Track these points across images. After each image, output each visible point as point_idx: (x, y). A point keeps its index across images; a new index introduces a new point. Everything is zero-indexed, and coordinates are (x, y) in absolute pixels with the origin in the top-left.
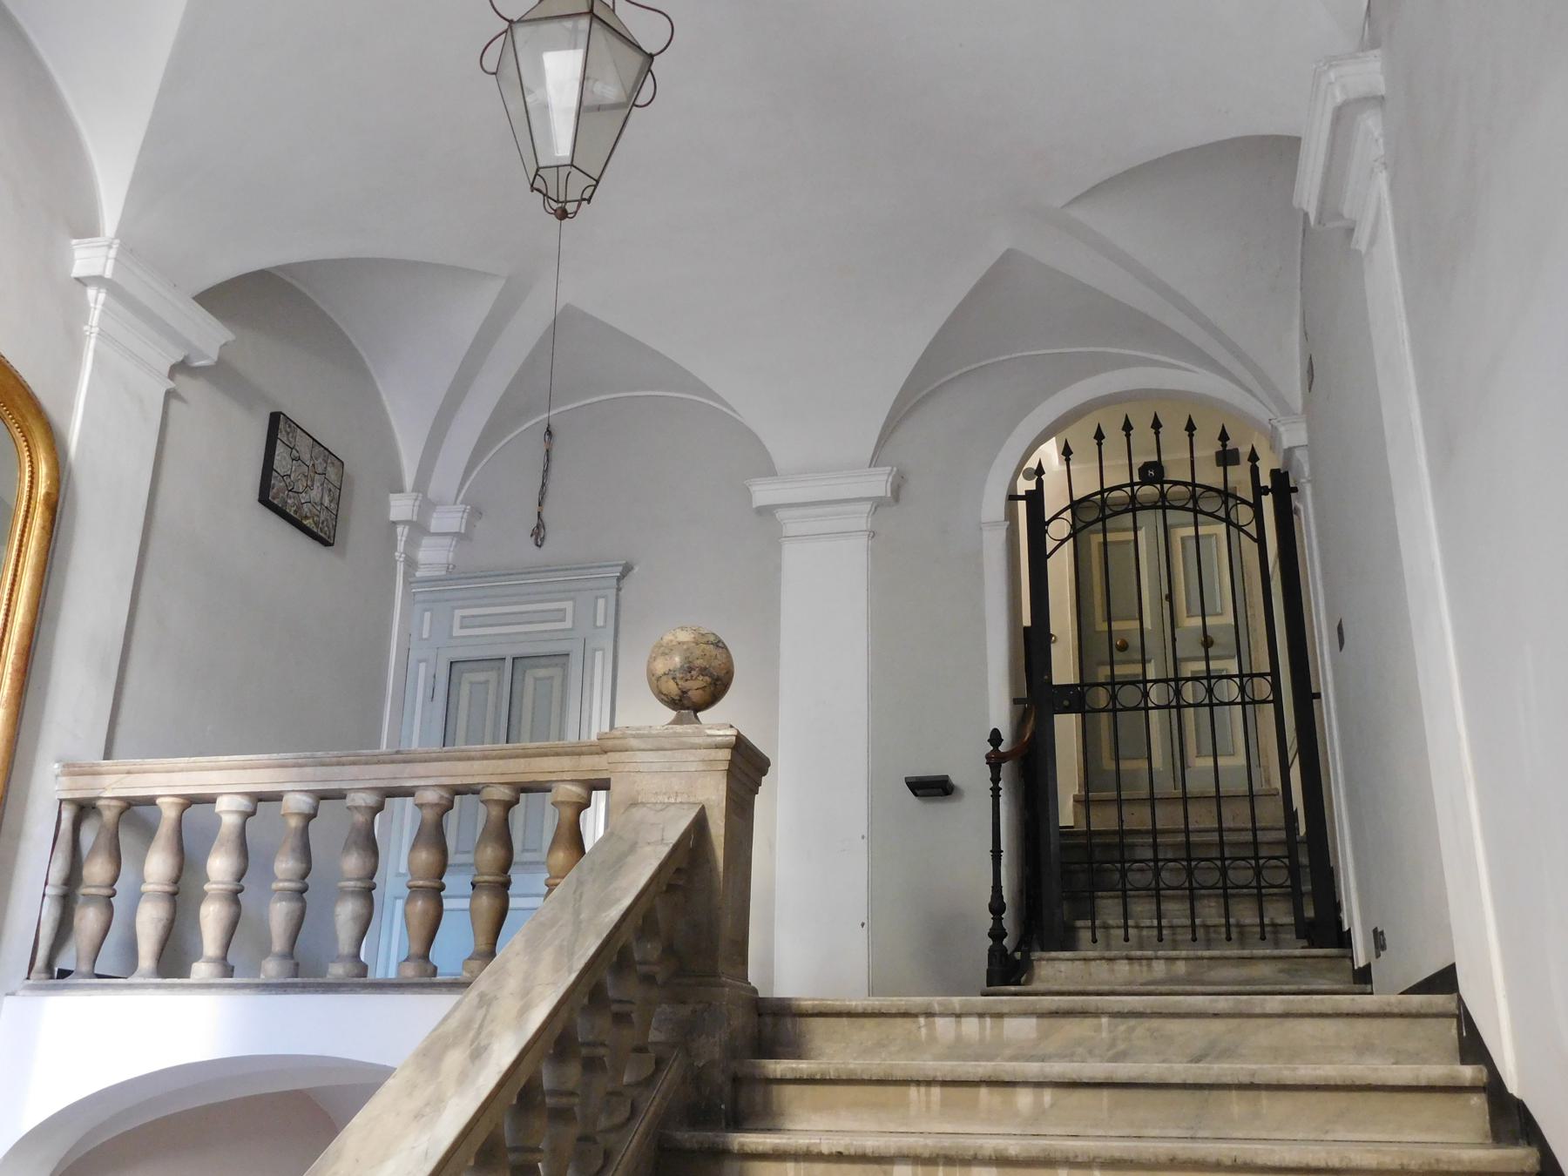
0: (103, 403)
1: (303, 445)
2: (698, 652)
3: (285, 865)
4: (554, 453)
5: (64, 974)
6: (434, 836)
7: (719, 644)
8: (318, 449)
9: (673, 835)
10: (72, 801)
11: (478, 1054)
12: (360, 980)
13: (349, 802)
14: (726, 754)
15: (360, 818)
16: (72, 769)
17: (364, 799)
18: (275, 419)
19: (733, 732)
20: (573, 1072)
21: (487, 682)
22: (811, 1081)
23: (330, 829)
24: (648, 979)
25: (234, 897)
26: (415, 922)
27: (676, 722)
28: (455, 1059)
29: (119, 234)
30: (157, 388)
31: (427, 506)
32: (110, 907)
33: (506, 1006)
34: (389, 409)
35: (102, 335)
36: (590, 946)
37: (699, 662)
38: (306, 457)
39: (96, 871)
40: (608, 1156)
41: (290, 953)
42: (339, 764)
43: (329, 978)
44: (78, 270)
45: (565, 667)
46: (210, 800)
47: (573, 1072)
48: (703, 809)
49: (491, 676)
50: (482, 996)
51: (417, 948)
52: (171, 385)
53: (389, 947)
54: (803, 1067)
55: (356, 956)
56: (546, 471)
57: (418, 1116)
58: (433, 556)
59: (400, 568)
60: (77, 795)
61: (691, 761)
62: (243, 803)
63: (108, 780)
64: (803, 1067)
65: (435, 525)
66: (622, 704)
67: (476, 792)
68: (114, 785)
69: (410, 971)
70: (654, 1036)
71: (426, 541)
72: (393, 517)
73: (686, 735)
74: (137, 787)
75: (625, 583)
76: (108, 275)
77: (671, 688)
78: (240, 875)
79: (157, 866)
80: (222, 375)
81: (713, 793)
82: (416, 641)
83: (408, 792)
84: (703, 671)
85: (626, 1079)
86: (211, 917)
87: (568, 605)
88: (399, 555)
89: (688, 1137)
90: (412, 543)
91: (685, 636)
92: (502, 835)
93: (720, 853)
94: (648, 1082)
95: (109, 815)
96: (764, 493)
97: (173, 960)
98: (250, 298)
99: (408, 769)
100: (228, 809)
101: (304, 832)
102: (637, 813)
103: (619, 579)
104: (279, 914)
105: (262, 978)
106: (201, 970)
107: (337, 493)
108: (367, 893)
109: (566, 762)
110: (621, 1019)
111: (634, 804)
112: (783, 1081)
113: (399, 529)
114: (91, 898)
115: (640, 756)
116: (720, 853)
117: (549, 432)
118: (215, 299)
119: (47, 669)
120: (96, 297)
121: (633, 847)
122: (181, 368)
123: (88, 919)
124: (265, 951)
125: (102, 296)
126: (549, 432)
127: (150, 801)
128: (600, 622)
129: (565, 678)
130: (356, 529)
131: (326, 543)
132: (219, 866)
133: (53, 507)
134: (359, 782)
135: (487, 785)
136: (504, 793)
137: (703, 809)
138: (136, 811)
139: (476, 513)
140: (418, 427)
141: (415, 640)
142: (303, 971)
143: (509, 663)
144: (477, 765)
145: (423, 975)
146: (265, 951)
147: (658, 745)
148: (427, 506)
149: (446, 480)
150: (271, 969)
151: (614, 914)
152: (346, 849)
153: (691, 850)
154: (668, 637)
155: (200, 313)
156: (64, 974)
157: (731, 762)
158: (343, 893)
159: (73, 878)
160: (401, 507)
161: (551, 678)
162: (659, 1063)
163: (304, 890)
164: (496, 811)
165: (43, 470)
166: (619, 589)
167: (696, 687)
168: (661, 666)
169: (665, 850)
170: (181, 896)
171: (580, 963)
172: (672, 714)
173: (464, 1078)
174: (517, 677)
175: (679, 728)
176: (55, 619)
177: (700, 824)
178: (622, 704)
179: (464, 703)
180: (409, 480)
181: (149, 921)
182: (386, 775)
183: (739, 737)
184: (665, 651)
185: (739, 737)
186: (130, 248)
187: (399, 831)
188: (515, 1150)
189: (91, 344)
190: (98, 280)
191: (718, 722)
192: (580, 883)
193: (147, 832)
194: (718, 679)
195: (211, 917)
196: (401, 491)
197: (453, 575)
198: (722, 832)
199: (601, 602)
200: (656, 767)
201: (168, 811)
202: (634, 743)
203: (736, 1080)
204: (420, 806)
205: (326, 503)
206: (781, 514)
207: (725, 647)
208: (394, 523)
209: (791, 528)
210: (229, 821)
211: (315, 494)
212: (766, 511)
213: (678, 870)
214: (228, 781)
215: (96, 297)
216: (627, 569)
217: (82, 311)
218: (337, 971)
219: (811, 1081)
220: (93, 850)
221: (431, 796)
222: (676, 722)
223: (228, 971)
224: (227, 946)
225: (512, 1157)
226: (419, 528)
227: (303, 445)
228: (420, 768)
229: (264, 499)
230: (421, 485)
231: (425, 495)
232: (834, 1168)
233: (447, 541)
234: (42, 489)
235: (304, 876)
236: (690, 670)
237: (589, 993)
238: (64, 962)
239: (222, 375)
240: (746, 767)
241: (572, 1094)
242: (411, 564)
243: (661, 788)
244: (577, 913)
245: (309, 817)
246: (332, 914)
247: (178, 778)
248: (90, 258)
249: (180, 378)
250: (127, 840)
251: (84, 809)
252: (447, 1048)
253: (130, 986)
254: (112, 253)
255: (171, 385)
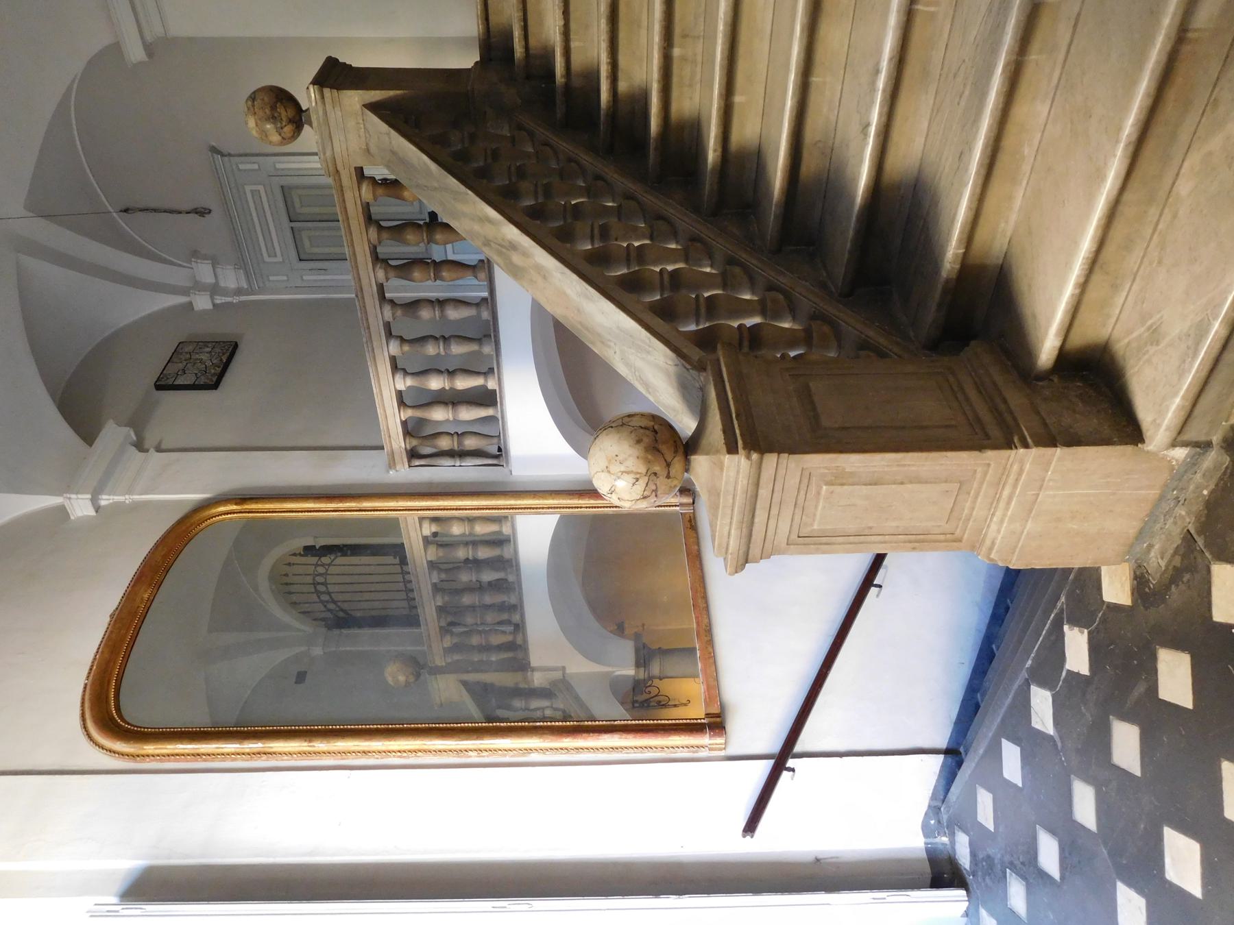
0: (171, 485)
1: (172, 369)
2: (261, 113)
3: (431, 349)
4: (142, 205)
5: (500, 449)
6: (406, 268)
7: (253, 97)
8: (174, 359)
9: (383, 127)
10: (409, 461)
11: (513, 247)
12: (489, 302)
13: (391, 320)
14: (327, 91)
15: (399, 312)
16: (392, 464)
17: (388, 312)
18: (159, 387)
19: (311, 88)
20: (525, 186)
21: (309, 238)
22: (525, 28)
23: (405, 326)
24: (473, 137)
25: (451, 373)
26: (454, 275)
27: (311, 125)
28: (516, 259)
29: (60, 494)
30: (155, 458)
31: (198, 287)
32: (463, 434)
33: (489, 231)
34: (137, 317)
35: (130, 492)
36: (452, 182)
37: (268, 111)
38: (181, 366)
39: (445, 443)
40: (570, 160)
41: (479, 341)
42: (369, 328)
43: (490, 318)
44: (92, 512)
45: (290, 188)
46: (400, 394)
47: (525, 186)
48: (364, 106)
49: (305, 235)
50: (485, 245)
51: (470, 272)
52: (152, 450)
53: (473, 289)
54: (517, 34)
55: (477, 305)
56: (155, 210)
57: (545, 277)
58: (231, 279)
59: (243, 298)
60: (405, 460)
61: (335, 115)
62: (399, 377)
63: (395, 446)
64: (517, 34)
65: (210, 280)
66: (307, 156)
67: (375, 247)
68: (397, 441)
69: (482, 275)
70: (506, 132)
71: (222, 284)
72: (210, 306)
73: (318, 119)
74: (396, 430)
75: (225, 150)
76: (89, 496)
77: (288, 129)
78: (439, 372)
79: (439, 414)
80: (138, 423)
81: (354, 99)
82: (288, 284)
83: (381, 288)
84: (273, 108)
85: (531, 150)
86: (463, 383)
87: (248, 189)
88: (236, 300)
89: (560, 111)
90: (225, 292)
91: (252, 123)
92: (401, 229)
93: (392, 93)
94: (531, 135)
95: (415, 442)
96: (135, 52)
97: (488, 398)
98: (81, 407)
99: (365, 287)
100: (403, 383)
101: (411, 342)
102: (373, 149)
103: (223, 155)
104: (457, 349)
105: (493, 353)
106: (491, 384)
107: (201, 344)
108: (441, 303)
109: (349, 195)
110: (495, 155)
111: (368, 150)
112: (527, 47)
113: (218, 302)
114: (460, 443)
115: (337, 149)
116: (392, 93)
117: (126, 211)
118: (88, 434)
119: (344, 486)
120: (105, 500)
121: (393, 153)
122: (140, 446)
123: (470, 443)
124: (479, 353)
125: (104, 497)
126: (126, 211)
127: (404, 424)
128: (256, 166)
129: (297, 187)
130: (225, 328)
131: (236, 346)
132: (435, 383)
133: (242, 499)
134: (377, 316)
135: (369, 241)
136: (373, 233)
137: (364, 106)
138: (409, 430)
139: (195, 254)
140: (143, 297)
141: (288, 284)
142: (488, 333)
143: (293, 224)
144: (358, 249)
145: (484, 267)
146: (479, 353)
147: (327, 137)
148: (198, 287)
149: (176, 276)
150: (488, 349)
151: (433, 166)
152: (418, 318)
153: (392, 114)
154: (254, 133)
155: (98, 442)
156: (500, 449)
157: (332, 87)
158: (443, 316)
159: (451, 454)
160: (202, 303)
161: (300, 196)
162: (520, 127)
163: (443, 337)
164: (385, 235)
165: (222, 509)
166: (230, 155)
167: (285, 113)
168: (275, 138)
169: (393, 132)
170: (452, 399)
171: (462, 188)
172: (306, 127)
173: (525, 254)
174: (302, 218)
175: (315, 124)
176: (310, 487)
177: (374, 107)
178: (307, 156)
179: (327, 250)
180: (182, 299)
181: (468, 414)
182: (372, 301)
183: (314, 82)
184: (264, 134)
185: (314, 82)
186: (67, 486)
187: (401, 290)
188: (565, 218)
189: (136, 497)
190: (94, 501)
191: (307, 97)
192: (418, 186)
193: (422, 422)
194: (277, 97)
195: (463, 383)
196: (191, 303)
197: (241, 264)
198: (378, 92)
199: (242, 167)
200: (342, 138)
201: (408, 413)
202: (329, 153)
203: (528, 77)
204: (387, 279)
205: (209, 349)
206: (149, 38)
207: (254, 93)
208: (214, 305)
209: (159, 30)
210: (409, 382)
211: (204, 357)
212: (149, 49)
213: (406, 122)
214: (387, 388)
215: (105, 500)
216: (214, 150)
217: (116, 506)
218: (485, 315)
219: (525, 28)
220: (435, 447)
221: (381, 274)
222: (311, 125)
223: (491, 370)
224: (478, 373)
225: (569, 221)
226: (214, 290)
227: (172, 369)
228: (365, 282)
229: (215, 386)
230: (185, 291)
231: (191, 288)
232: (572, 16)
233: (219, 271)
234: (234, 507)
235: (436, 338)
236: (274, 117)
237: (477, 180)
238: (493, 450)
239: (138, 423)
240: (335, 75)
241: (536, 185)
242: (239, 292)
243: (351, 134)
244: (436, 189)
245: (402, 340)
246: (457, 322)
247: (389, 412)
248: (80, 507)
249: (146, 446)
250: (429, 431)
251: (413, 455)
252: (511, 263)
253: (503, 418)
254: (73, 496)
255: (152, 450)
